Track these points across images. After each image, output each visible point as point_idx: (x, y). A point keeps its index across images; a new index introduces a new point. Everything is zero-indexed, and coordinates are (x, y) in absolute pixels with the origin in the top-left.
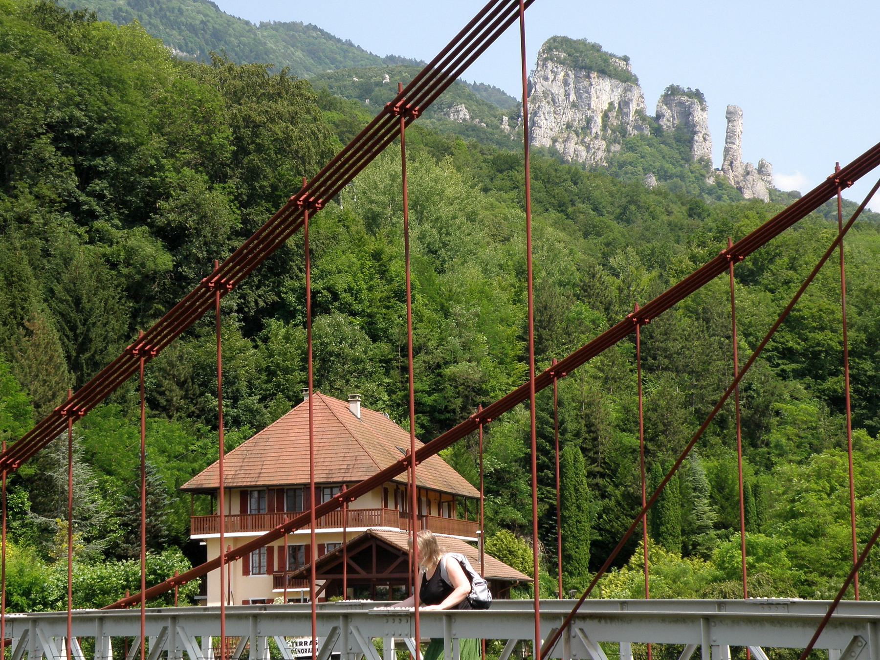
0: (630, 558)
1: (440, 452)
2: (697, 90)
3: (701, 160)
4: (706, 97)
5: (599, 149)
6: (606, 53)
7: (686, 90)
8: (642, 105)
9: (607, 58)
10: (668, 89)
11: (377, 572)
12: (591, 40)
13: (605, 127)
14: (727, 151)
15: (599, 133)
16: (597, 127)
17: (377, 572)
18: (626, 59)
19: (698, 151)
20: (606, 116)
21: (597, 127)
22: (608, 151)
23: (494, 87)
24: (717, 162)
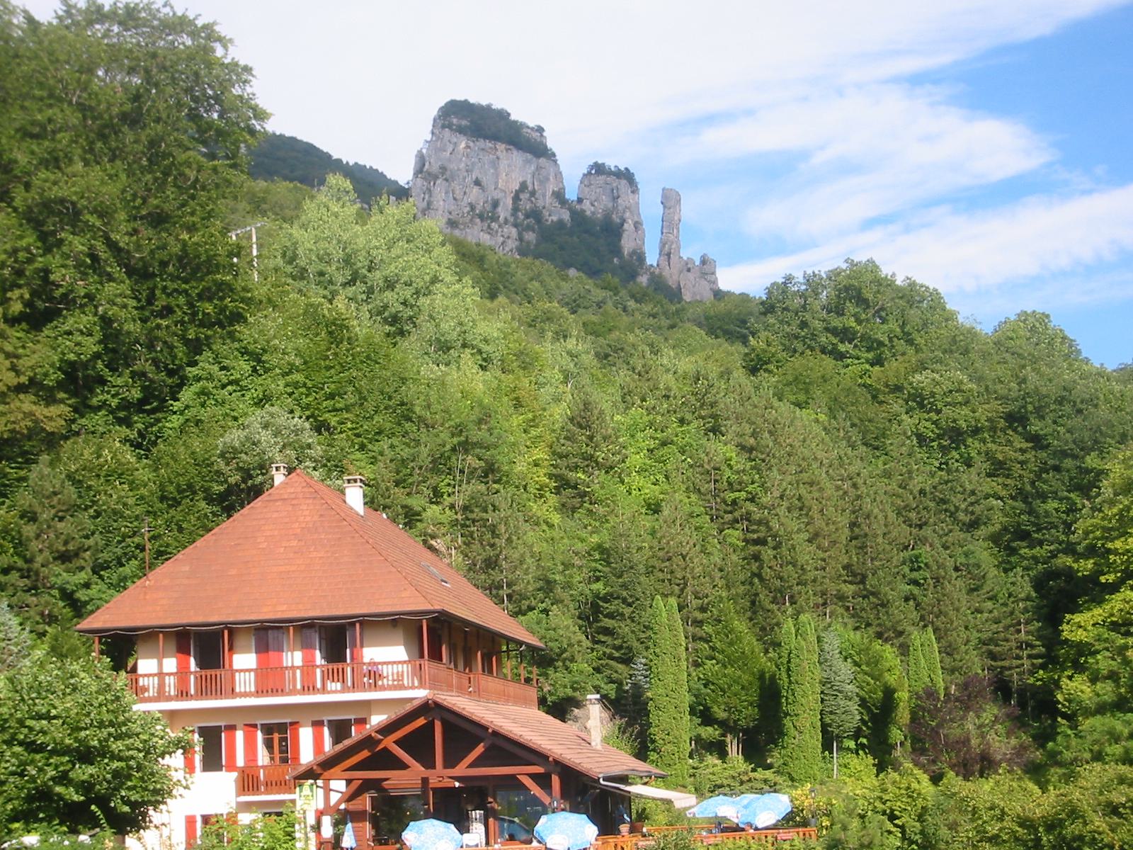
0: (593, 819)
1: (340, 795)
2: (626, 169)
3: (634, 252)
4: (637, 178)
5: (508, 237)
6: (515, 122)
7: (613, 169)
8: (561, 186)
9: (517, 127)
10: (592, 167)
11: (445, 767)
12: (497, 105)
13: (516, 209)
14: (663, 244)
15: (509, 218)
16: (503, 212)
17: (445, 767)
18: (540, 130)
19: (627, 245)
20: (516, 198)
21: (503, 212)
22: (521, 239)
23: (371, 167)
24: (652, 258)
